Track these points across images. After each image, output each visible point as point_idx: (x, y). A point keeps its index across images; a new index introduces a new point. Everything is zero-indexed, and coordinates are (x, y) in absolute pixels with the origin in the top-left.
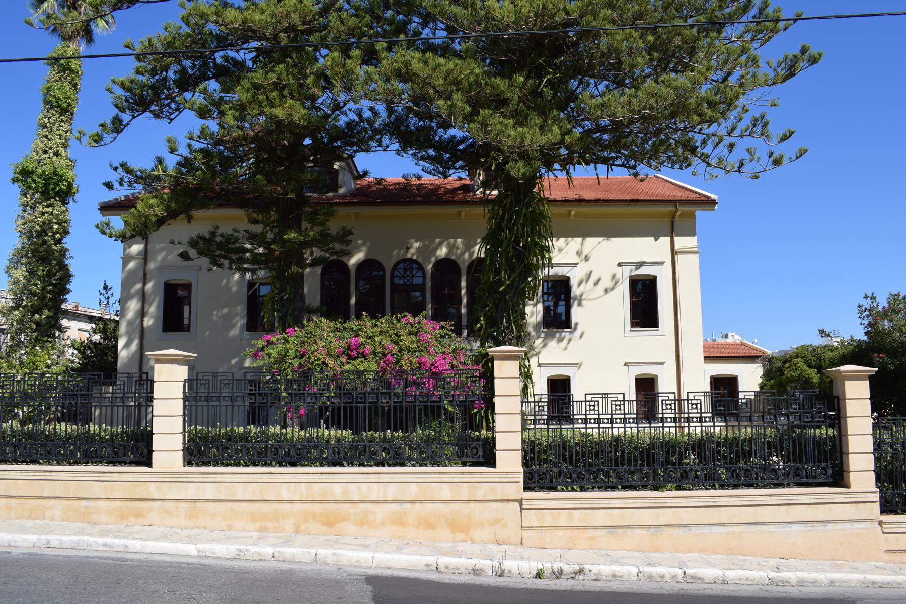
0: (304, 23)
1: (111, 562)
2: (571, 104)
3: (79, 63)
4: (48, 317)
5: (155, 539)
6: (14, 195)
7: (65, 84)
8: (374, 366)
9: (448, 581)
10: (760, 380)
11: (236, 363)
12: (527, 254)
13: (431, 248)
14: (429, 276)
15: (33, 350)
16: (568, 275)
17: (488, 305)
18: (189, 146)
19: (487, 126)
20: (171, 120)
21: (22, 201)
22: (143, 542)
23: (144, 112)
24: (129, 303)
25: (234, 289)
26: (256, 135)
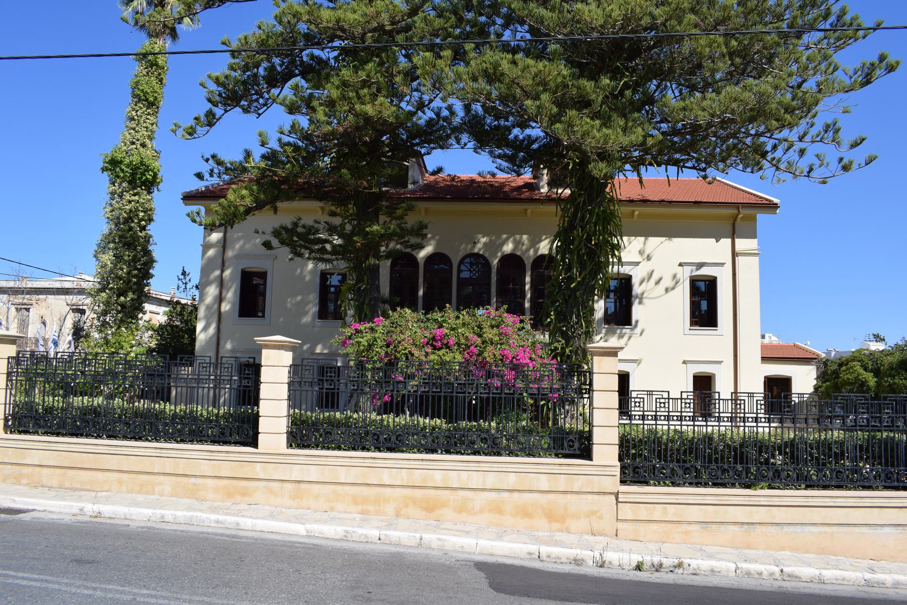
0: (393, 23)
1: (226, 538)
2: (647, 107)
3: (165, 59)
4: (132, 299)
5: (264, 518)
6: (103, 183)
7: (152, 78)
8: (459, 358)
9: (553, 570)
10: (815, 382)
11: (308, 349)
12: (598, 252)
13: (497, 243)
14: (494, 270)
15: (118, 331)
16: (630, 273)
17: (558, 301)
18: (280, 140)
19: (573, 126)
20: (260, 115)
21: (111, 189)
22: (254, 521)
23: (235, 107)
24: (208, 289)
25: (308, 278)
26: (345, 130)
